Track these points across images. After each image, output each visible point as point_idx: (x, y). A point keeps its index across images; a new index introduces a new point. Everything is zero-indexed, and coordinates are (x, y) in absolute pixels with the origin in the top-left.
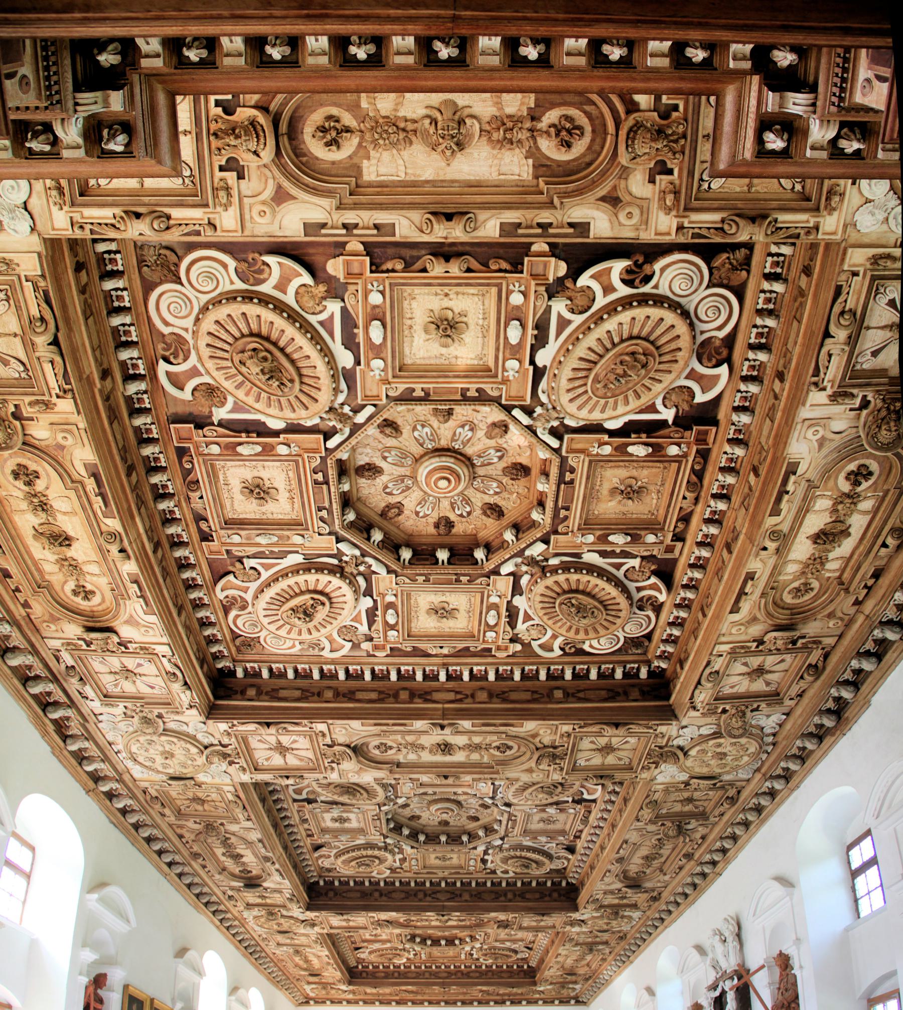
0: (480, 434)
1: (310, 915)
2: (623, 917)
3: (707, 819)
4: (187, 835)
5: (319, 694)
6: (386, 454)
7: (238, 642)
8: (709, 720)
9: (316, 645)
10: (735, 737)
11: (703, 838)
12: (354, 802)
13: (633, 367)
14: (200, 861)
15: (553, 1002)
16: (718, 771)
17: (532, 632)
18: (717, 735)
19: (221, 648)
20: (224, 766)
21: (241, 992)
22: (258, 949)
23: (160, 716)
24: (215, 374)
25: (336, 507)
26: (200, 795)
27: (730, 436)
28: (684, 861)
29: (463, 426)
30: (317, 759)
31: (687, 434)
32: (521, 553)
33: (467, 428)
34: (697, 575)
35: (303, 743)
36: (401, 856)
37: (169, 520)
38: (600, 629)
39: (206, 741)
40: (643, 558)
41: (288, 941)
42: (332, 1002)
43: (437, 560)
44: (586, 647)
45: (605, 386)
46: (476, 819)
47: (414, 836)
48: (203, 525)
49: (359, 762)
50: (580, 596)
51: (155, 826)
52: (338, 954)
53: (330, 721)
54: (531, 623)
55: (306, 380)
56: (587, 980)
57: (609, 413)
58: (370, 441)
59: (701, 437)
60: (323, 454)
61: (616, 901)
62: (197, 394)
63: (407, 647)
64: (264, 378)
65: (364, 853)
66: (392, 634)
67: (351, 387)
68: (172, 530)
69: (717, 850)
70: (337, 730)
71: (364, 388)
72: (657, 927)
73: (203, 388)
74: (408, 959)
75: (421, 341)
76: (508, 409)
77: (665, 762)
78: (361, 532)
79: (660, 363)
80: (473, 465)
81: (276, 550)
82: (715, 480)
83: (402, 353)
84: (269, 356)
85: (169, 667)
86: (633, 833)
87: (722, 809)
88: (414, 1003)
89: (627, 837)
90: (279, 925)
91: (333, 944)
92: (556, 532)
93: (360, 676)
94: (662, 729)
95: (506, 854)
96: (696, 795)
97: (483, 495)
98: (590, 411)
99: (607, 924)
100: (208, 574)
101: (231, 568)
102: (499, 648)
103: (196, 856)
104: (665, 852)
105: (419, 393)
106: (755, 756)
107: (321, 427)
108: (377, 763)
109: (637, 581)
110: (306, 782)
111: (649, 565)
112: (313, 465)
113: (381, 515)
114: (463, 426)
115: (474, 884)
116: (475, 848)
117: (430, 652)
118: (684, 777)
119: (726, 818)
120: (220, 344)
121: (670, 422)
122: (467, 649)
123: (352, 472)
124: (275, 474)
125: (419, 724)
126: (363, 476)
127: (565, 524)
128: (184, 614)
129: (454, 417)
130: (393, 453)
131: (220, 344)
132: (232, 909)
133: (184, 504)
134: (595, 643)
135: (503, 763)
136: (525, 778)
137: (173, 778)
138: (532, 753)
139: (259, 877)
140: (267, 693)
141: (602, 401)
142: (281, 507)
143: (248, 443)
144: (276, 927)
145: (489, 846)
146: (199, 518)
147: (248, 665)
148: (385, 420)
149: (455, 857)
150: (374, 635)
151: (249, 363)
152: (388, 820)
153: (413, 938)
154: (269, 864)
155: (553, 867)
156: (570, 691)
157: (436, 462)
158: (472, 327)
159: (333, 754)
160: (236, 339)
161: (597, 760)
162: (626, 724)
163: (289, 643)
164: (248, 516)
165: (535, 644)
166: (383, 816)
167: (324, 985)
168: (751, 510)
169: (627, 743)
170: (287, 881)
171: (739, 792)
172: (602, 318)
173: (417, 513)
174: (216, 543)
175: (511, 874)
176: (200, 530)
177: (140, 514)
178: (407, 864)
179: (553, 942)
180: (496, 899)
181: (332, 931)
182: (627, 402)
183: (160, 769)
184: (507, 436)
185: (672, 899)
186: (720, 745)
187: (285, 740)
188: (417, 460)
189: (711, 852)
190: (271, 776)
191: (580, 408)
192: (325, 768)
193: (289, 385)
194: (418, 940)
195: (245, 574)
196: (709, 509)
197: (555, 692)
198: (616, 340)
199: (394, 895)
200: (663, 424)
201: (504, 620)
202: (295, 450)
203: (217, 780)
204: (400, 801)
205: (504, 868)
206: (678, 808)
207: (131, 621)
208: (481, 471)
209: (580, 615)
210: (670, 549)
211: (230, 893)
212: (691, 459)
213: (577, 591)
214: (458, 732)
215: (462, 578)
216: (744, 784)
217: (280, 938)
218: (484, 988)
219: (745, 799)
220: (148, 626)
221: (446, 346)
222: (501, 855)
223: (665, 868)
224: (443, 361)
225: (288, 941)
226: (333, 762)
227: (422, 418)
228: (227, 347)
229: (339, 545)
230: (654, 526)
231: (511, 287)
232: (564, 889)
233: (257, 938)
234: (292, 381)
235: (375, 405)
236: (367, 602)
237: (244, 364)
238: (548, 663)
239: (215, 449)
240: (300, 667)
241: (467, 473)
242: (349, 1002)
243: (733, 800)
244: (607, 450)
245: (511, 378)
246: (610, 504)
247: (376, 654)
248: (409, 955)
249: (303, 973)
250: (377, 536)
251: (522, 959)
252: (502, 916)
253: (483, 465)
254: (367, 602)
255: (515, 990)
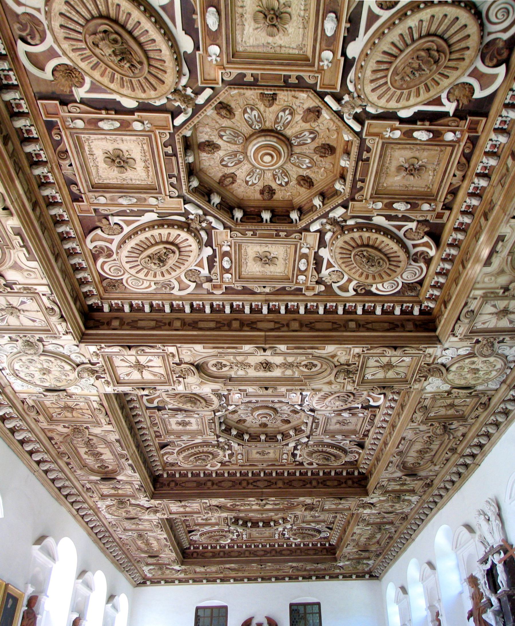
0: (298, 118)
1: (155, 502)
2: (404, 501)
3: (466, 420)
4: (56, 437)
5: (170, 324)
6: (222, 133)
7: (105, 283)
8: (465, 343)
9: (168, 285)
10: (485, 356)
11: (464, 435)
12: (195, 409)
13: (427, 62)
14: (65, 459)
15: (351, 577)
16: (473, 382)
17: (333, 276)
18: (471, 355)
19: (91, 289)
20: (92, 380)
21: (88, 575)
22: (107, 534)
23: (40, 340)
24: (72, 55)
25: (183, 175)
26: (70, 404)
27: (496, 127)
28: (450, 454)
29: (284, 111)
30: (168, 375)
31: (462, 123)
32: (325, 215)
33: (287, 112)
34: (460, 236)
35: (157, 362)
36: (230, 452)
37: (44, 184)
38: (384, 275)
39: (78, 361)
40: (419, 222)
41: (134, 527)
42: (166, 582)
43: (262, 219)
44: (373, 289)
45: (402, 79)
46: (288, 422)
47: (240, 436)
48: (74, 189)
49: (200, 377)
50: (370, 250)
51: (31, 430)
52: (175, 537)
53: (179, 345)
54: (332, 269)
55: (153, 63)
56: (378, 556)
57: (403, 103)
58: (209, 121)
59: (473, 126)
60: (172, 131)
61: (398, 487)
62: (57, 74)
63: (238, 286)
64: (116, 59)
65: (201, 450)
66: (227, 276)
67: (192, 72)
68: (47, 192)
69: (475, 445)
70: (184, 352)
71: (203, 72)
72: (432, 509)
73: (62, 68)
74: (232, 540)
75: (251, 30)
76: (321, 96)
77: (432, 376)
78: (204, 196)
79: (449, 60)
80: (291, 145)
81: (135, 209)
82: (482, 162)
83: (234, 40)
84: (119, 38)
85: (48, 304)
86: (410, 431)
87: (477, 412)
88: (236, 580)
89: (404, 435)
90: (127, 512)
91: (171, 528)
92: (353, 199)
93: (202, 310)
94: (430, 351)
95: (311, 449)
96: (457, 402)
97: (298, 169)
98: (388, 101)
99: (392, 506)
100: (79, 229)
101: (98, 224)
102: (308, 289)
103: (61, 455)
104: (435, 447)
105: (249, 79)
106: (501, 371)
107: (168, 107)
108: (214, 378)
109: (414, 240)
110: (158, 393)
111: (423, 227)
112: (164, 140)
113: (219, 183)
114: (284, 111)
115: (286, 474)
116: (287, 445)
117: (256, 290)
118: (446, 387)
119: (481, 419)
120: (73, 26)
121: (451, 114)
122: (284, 288)
123: (196, 147)
124: (132, 147)
125: (247, 348)
126: (204, 151)
127: (361, 193)
128: (60, 261)
129: (277, 102)
130: (228, 132)
131: (73, 26)
132: (88, 500)
133: (56, 171)
134: (380, 286)
135: (309, 377)
136: (326, 389)
137: (48, 390)
138: (332, 370)
139: (114, 471)
140: (128, 324)
141: (399, 92)
142: (138, 174)
143: (108, 119)
144: (124, 514)
145: (298, 443)
146: (70, 183)
147: (113, 302)
148: (220, 103)
149: (272, 453)
150: (213, 277)
151: (101, 44)
152: (220, 423)
153: (236, 521)
154: (123, 460)
155: (347, 459)
156: (361, 323)
157: (262, 141)
158: (294, 18)
159: (178, 370)
160: (88, 21)
161: (380, 375)
162: (403, 347)
163: (146, 284)
164: (111, 182)
165: (335, 286)
166: (217, 420)
167: (161, 566)
168: (506, 187)
169: (403, 361)
170: (137, 475)
171: (490, 399)
172: (406, 14)
173: (247, 182)
174: (85, 203)
175: (315, 466)
176: (71, 193)
177: (18, 177)
178: (234, 458)
179: (349, 522)
180: (304, 486)
181: (171, 516)
182: (418, 94)
183: (38, 383)
184: (320, 121)
185: (442, 485)
186: (473, 363)
187: (143, 360)
188: (248, 139)
189: (470, 446)
190: (130, 388)
191: (379, 98)
192: (174, 382)
193: (139, 66)
194: (241, 522)
195: (110, 229)
196: (473, 185)
197: (350, 323)
198: (416, 36)
199: (223, 484)
200: (446, 114)
201: (312, 266)
202: (148, 126)
203: (86, 392)
204: (231, 408)
205: (310, 462)
206: (443, 412)
207: (16, 267)
208: (297, 150)
209: (369, 264)
210: (440, 216)
211: (88, 486)
212: (462, 144)
213: (368, 246)
214: (276, 354)
215: (280, 233)
216: (493, 392)
217: (127, 524)
218: (294, 564)
219: (495, 405)
220: (30, 271)
221: (272, 35)
222: (307, 450)
223: (435, 460)
224: (269, 49)
225: (134, 527)
226: (180, 377)
227: (251, 102)
228: (80, 29)
229: (186, 206)
230: (428, 197)
231: (302, 245)
232: (356, 477)
233: (107, 524)
234: (141, 63)
235: (212, 88)
236: (208, 251)
237: (97, 46)
238: (345, 301)
239: (80, 124)
240: (154, 303)
241: (286, 151)
242: (180, 581)
243: (485, 406)
244: (397, 134)
245: (325, 68)
246: (396, 178)
247: (215, 292)
248: (234, 536)
249: (143, 555)
250: (216, 200)
251: (325, 538)
252: (308, 500)
253: (299, 145)
254: (208, 251)
255: (319, 566)
